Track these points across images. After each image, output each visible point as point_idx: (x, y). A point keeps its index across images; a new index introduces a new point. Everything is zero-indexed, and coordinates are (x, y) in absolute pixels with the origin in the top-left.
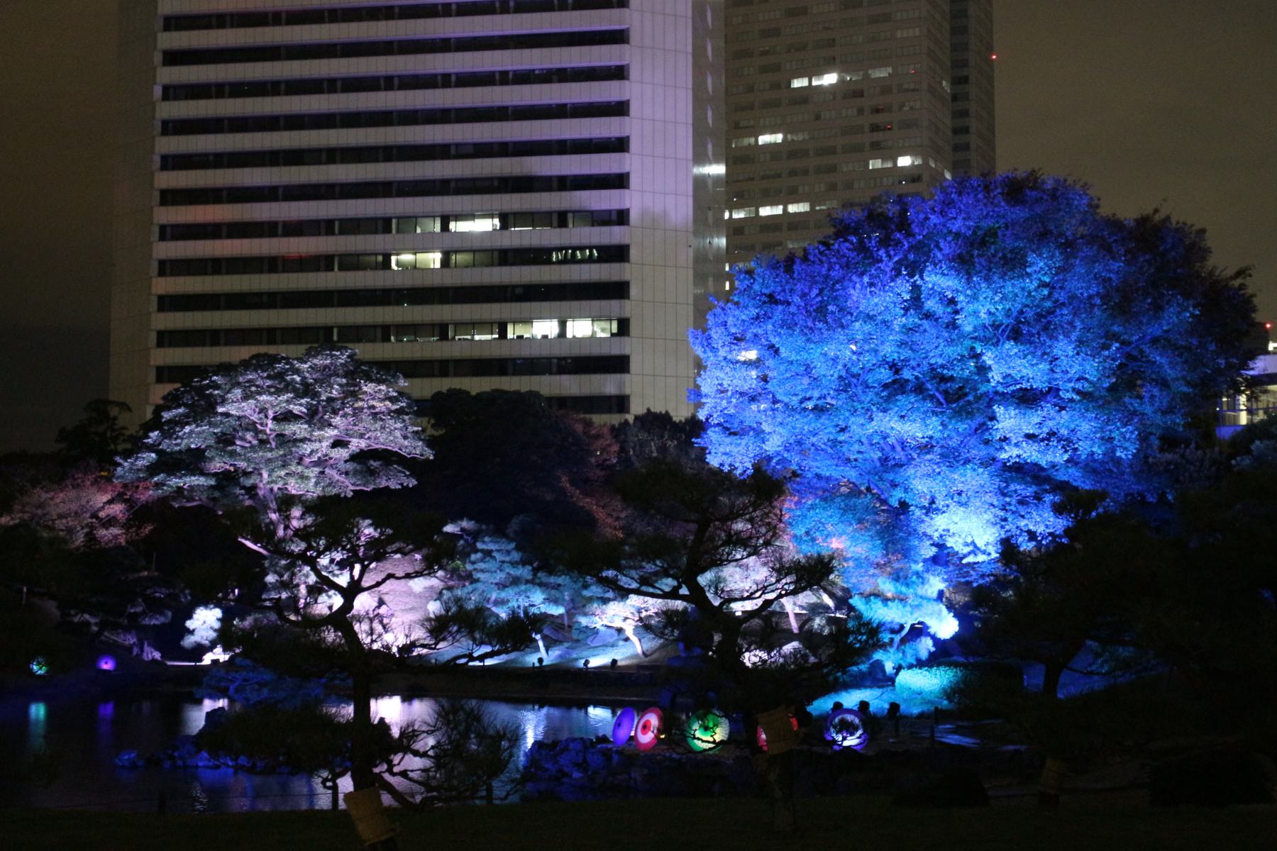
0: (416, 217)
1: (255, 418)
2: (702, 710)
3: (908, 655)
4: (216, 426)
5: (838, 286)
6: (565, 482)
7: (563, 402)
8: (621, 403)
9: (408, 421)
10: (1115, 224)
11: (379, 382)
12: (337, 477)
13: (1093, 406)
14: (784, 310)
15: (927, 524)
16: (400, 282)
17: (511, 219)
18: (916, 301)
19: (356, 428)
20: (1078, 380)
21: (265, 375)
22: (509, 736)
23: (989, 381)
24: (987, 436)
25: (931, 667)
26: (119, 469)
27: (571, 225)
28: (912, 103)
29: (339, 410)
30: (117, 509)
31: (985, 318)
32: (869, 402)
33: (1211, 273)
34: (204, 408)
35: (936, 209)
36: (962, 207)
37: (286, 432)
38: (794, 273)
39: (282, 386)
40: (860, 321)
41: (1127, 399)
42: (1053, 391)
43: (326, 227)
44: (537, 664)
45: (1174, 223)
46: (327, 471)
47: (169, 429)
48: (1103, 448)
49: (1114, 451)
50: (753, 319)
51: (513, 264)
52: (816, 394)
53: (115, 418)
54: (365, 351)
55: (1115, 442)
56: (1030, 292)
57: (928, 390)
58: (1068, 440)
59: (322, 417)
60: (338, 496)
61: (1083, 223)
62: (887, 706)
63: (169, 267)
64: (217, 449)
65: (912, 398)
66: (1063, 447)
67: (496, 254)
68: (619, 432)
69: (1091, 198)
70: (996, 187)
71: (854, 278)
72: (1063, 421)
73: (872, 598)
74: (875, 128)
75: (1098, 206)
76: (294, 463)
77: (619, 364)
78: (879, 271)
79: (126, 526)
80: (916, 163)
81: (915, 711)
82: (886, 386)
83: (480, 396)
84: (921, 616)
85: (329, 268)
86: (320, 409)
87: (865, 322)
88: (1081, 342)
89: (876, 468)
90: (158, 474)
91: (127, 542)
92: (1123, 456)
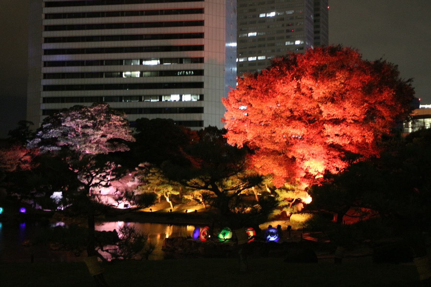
0: (131, 60)
1: (74, 127)
2: (221, 228)
3: (295, 209)
4: (61, 130)
5: (272, 83)
6: (181, 149)
7: (180, 123)
8: (200, 123)
9: (127, 129)
10: (367, 63)
11: (117, 115)
12: (103, 147)
13: (359, 125)
14: (254, 91)
15: (302, 164)
16: (126, 82)
17: (164, 61)
18: (299, 89)
19: (109, 131)
20: (353, 116)
21: (78, 112)
22: (145, 237)
23: (322, 116)
24: (322, 135)
25: (302, 213)
26: (28, 144)
27: (184, 63)
28: (300, 23)
29: (104, 124)
30: (28, 158)
31: (322, 95)
32: (282, 123)
33: (400, 80)
34: (57, 123)
35: (306, 57)
36: (315, 57)
37: (86, 132)
38: (257, 79)
39: (84, 116)
40: (280, 95)
41: (370, 123)
42: (344, 120)
43: (100, 63)
44: (170, 211)
45: (387, 63)
46: (99, 145)
47: (45, 131)
48: (361, 139)
49: (365, 139)
50: (243, 94)
51: (164, 76)
52: (265, 120)
53: (28, 127)
54: (113, 105)
55: (365, 137)
56: (337, 86)
57: (303, 119)
58: (350, 137)
59: (98, 127)
60: (103, 154)
61: (356, 62)
62: (287, 227)
63: (47, 76)
64: (62, 137)
65: (297, 122)
66: (348, 138)
67: (158, 72)
68: (200, 133)
69: (359, 54)
70: (326, 50)
71: (278, 81)
72: (349, 130)
73: (283, 190)
74: (288, 31)
75: (361, 57)
76: (88, 143)
77: (200, 110)
78: (286, 78)
79: (31, 163)
80: (302, 43)
81: (297, 228)
82: (288, 118)
83: (153, 120)
84: (299, 196)
85: (102, 77)
86: (97, 124)
87: (281, 96)
88: (354, 103)
89: (285, 145)
90: (41, 146)
91: (31, 169)
92: (369, 142)
